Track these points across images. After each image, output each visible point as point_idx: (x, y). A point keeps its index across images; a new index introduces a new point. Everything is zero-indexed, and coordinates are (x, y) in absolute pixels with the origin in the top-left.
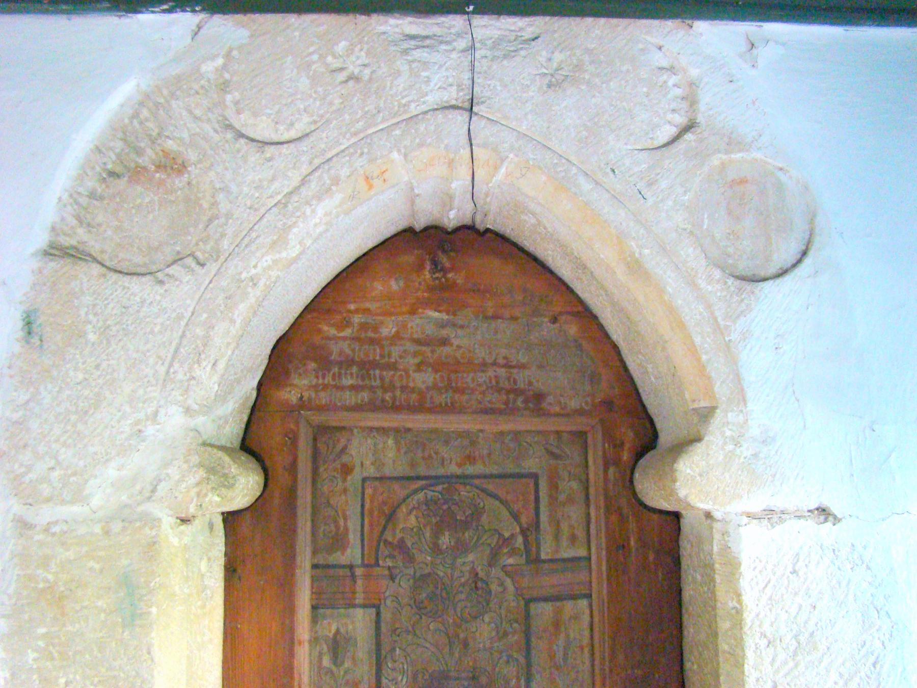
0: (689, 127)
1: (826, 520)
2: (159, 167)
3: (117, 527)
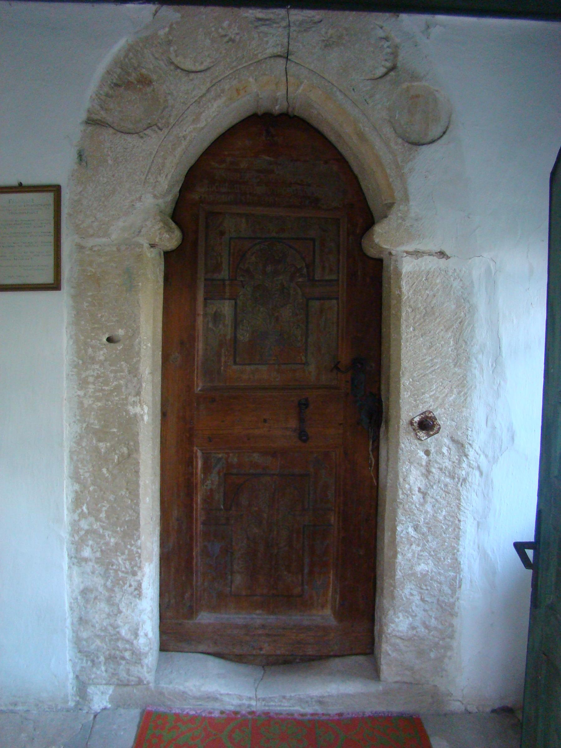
0: (393, 68)
1: (443, 257)
2: (139, 82)
3: (123, 248)
